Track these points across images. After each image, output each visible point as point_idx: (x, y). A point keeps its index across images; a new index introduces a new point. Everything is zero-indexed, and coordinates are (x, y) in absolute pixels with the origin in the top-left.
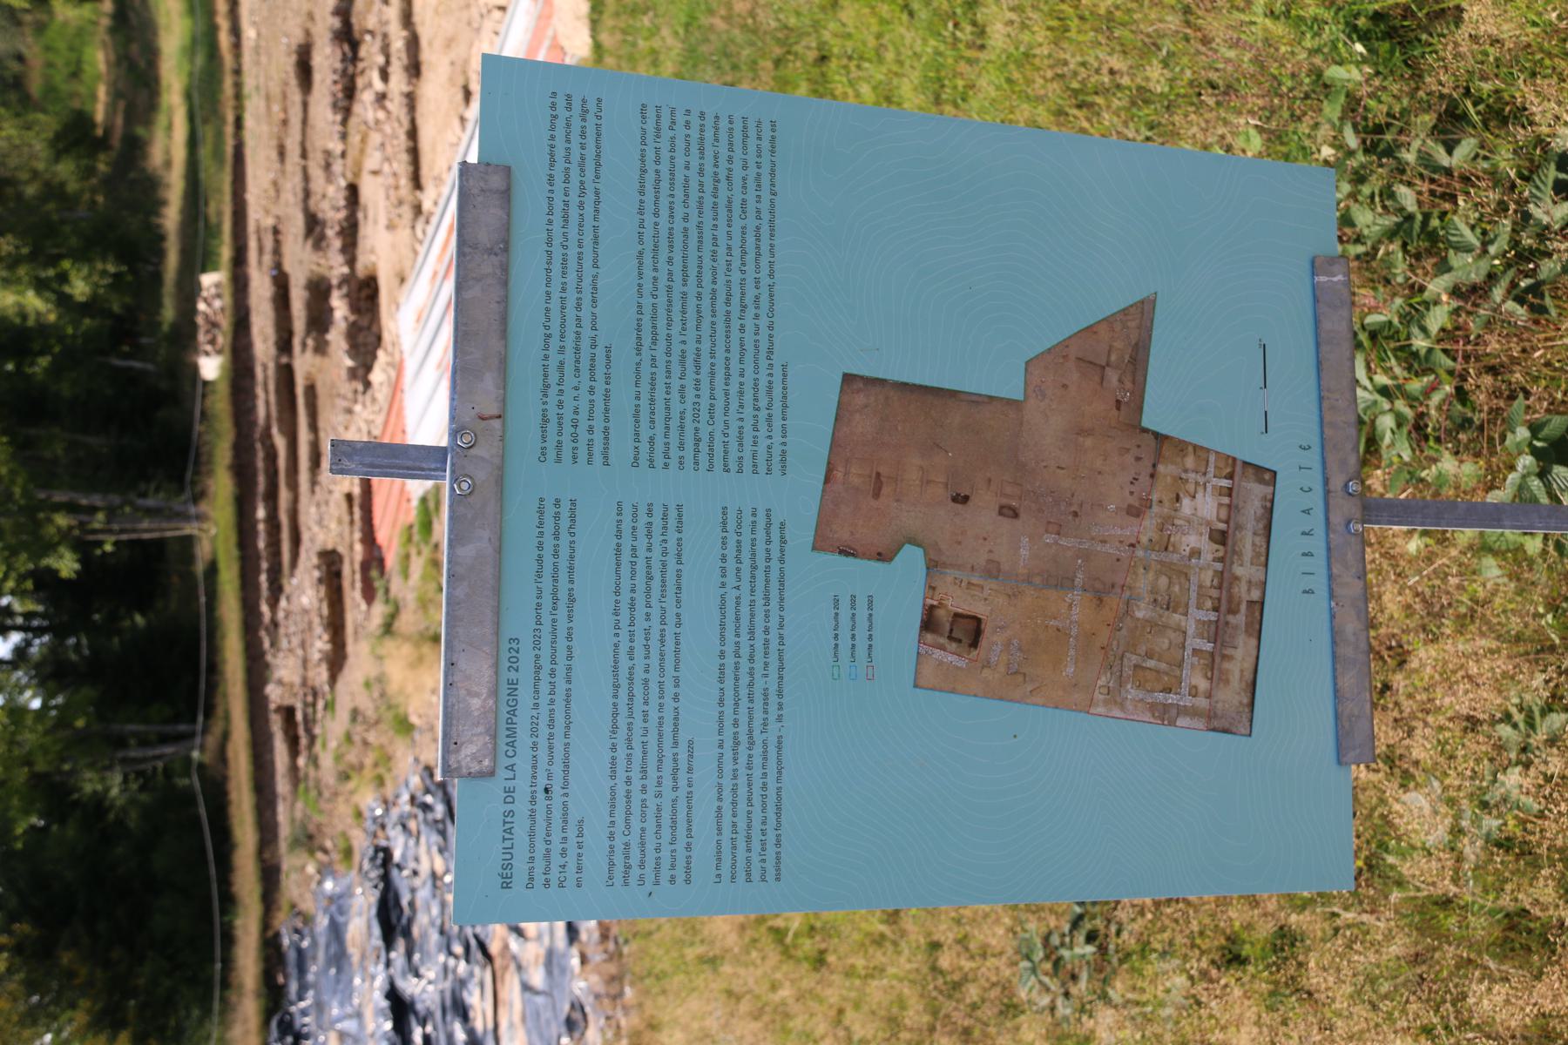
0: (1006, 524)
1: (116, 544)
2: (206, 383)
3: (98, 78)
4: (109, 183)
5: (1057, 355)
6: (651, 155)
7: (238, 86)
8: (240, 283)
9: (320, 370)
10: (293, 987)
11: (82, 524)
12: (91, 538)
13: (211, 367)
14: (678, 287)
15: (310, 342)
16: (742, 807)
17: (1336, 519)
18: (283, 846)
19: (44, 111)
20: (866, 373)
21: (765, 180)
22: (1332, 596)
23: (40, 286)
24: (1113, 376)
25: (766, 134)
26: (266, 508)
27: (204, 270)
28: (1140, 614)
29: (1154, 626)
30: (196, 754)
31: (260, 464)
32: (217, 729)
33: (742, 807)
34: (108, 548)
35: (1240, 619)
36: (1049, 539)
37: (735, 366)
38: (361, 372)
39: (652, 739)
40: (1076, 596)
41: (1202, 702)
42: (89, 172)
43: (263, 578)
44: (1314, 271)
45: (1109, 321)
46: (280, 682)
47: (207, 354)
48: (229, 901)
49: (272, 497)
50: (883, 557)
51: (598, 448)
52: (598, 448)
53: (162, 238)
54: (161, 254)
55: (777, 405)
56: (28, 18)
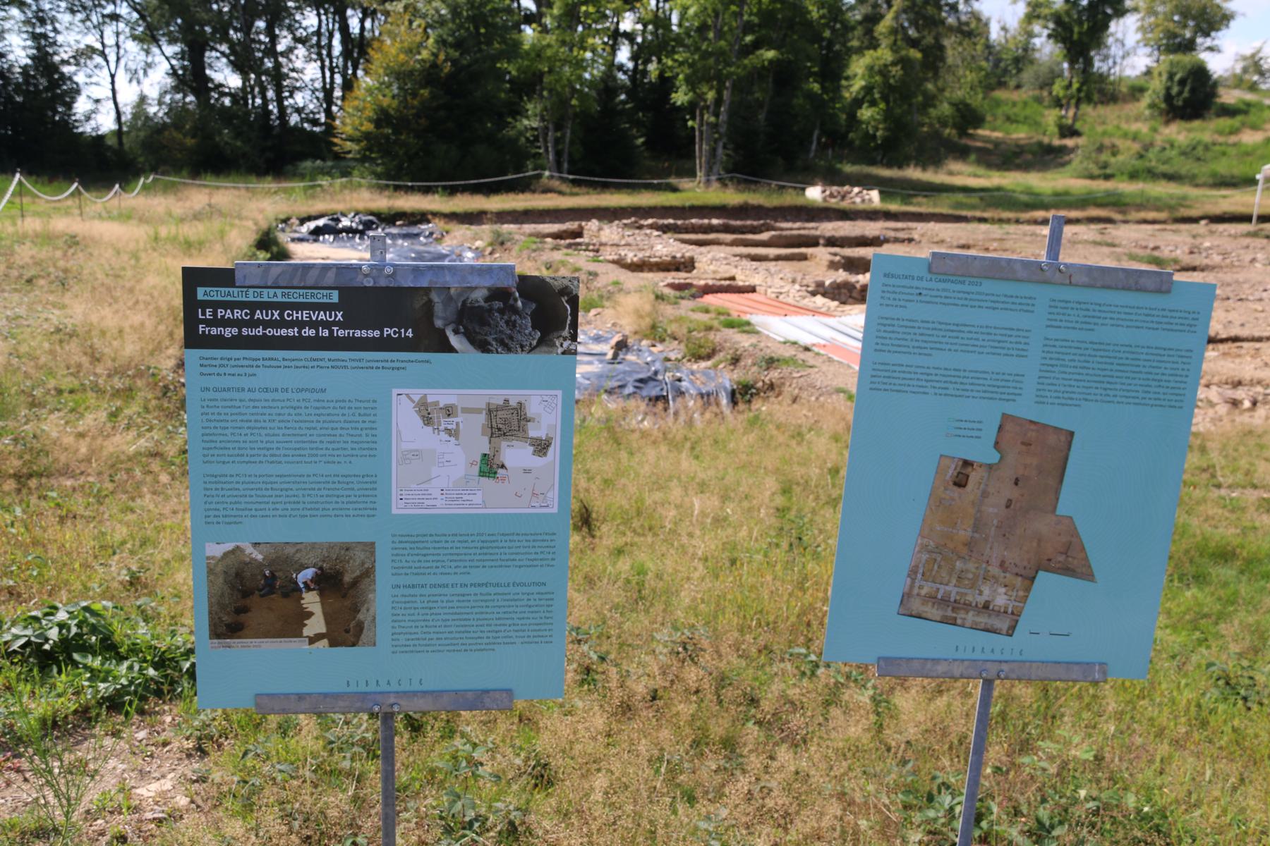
0: (1004, 502)
1: (693, 128)
2: (804, 189)
3: (1008, 133)
4: (936, 135)
5: (1074, 533)
6: (1171, 353)
7: (1008, 221)
8: (872, 215)
9: (818, 264)
10: (394, 231)
11: (708, 107)
12: (698, 113)
13: (814, 193)
14: (1116, 361)
15: (837, 258)
16: (902, 375)
17: (989, 665)
18: (497, 227)
19: (984, 98)
20: (1074, 441)
21: (1158, 402)
22: (955, 660)
23: (868, 89)
24: (1061, 558)
25: (1177, 404)
26: (720, 225)
27: (881, 193)
28: (958, 563)
29: (952, 570)
30: (547, 173)
31: (749, 222)
32: (564, 188)
33: (902, 375)
34: (690, 123)
35: (949, 613)
36: (995, 522)
37: (1082, 384)
38: (821, 290)
39: (935, 339)
40: (969, 533)
41: (916, 591)
42: (944, 123)
43: (671, 221)
44: (1101, 664)
45: (1086, 559)
46: (600, 229)
47: (824, 192)
48: (452, 191)
49: (726, 229)
50: (997, 445)
51: (1054, 323)
52: (1054, 323)
53: (900, 167)
54: (889, 165)
55: (1064, 401)
56: (1045, 93)
